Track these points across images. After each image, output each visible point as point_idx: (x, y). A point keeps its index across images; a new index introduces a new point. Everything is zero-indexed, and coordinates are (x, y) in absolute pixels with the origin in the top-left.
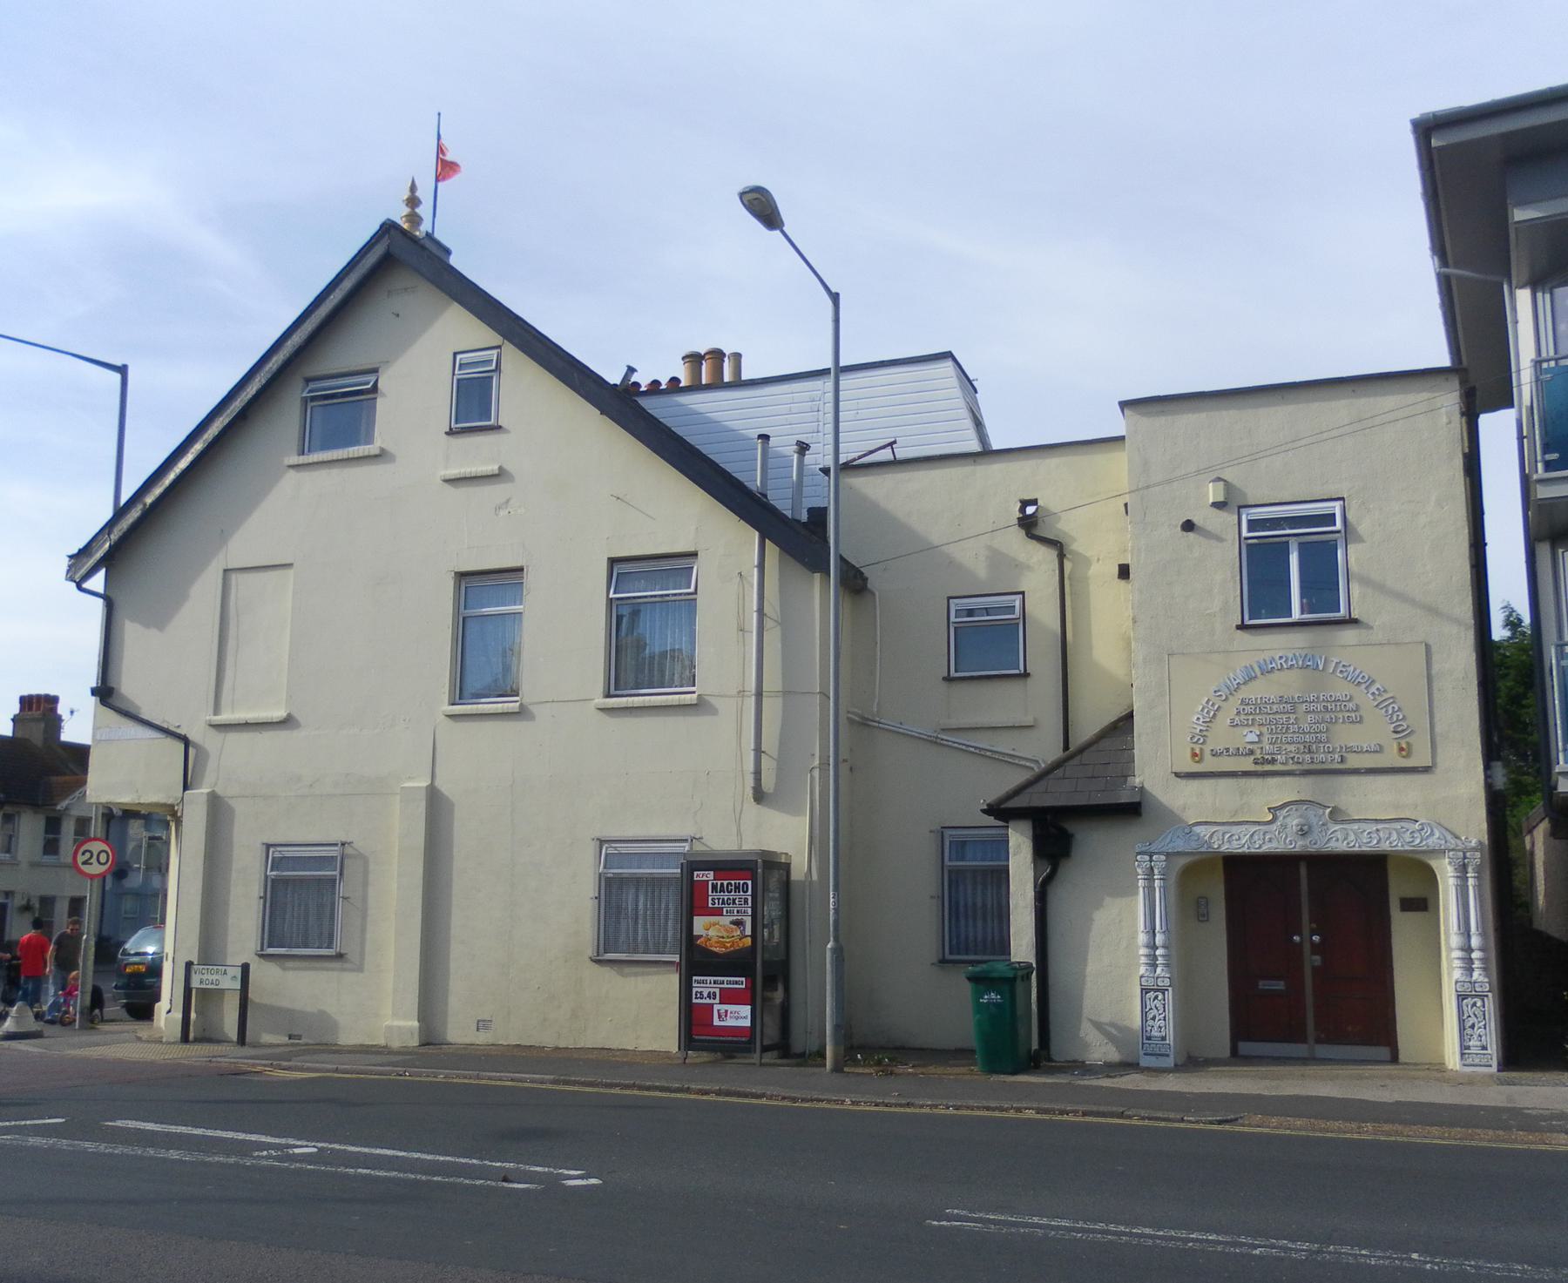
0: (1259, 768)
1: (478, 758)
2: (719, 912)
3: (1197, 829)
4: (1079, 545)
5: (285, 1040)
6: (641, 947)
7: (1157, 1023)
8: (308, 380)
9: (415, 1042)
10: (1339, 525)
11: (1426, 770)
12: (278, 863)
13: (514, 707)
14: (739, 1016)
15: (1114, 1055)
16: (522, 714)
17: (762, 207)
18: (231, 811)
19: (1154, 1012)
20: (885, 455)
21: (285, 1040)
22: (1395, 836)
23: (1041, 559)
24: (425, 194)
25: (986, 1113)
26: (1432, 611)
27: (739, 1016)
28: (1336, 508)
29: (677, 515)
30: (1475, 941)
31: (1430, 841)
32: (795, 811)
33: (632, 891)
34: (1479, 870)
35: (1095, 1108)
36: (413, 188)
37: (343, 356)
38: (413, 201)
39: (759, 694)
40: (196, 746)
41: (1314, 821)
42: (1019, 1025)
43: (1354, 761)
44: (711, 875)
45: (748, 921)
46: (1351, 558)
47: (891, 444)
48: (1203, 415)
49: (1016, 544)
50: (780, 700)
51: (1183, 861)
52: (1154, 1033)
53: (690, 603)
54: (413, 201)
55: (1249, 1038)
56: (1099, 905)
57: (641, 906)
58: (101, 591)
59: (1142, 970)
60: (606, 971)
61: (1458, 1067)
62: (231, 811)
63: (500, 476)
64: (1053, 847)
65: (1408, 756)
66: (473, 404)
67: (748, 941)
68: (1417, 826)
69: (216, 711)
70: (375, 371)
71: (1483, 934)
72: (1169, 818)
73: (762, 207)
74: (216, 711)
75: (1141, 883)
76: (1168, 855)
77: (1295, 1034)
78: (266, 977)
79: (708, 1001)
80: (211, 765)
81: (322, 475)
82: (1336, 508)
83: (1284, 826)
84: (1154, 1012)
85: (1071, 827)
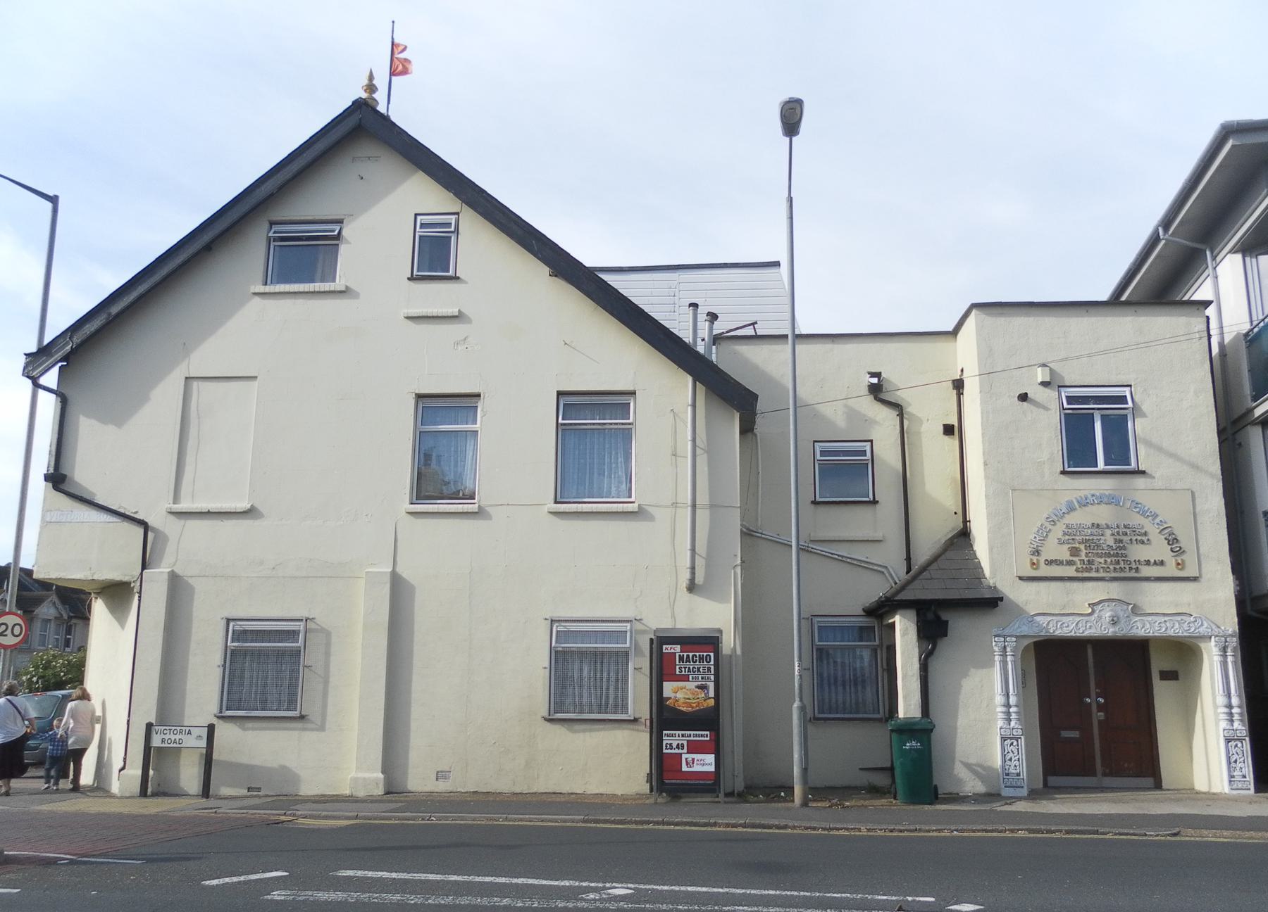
0: (1080, 575)
1: (437, 550)
2: (685, 678)
3: (1038, 619)
4: (912, 409)
5: (244, 792)
6: (586, 708)
7: (1013, 763)
8: (272, 224)
9: (380, 791)
10: (1130, 404)
11: (1195, 579)
12: (241, 635)
13: (474, 508)
14: (705, 763)
15: (980, 788)
16: (479, 514)
17: (791, 117)
18: (191, 590)
19: (1011, 755)
20: (749, 331)
21: (244, 792)
22: (1177, 626)
23: (886, 417)
24: (381, 82)
25: (985, 834)
26: (1195, 467)
27: (705, 763)
28: (1127, 391)
29: (616, 360)
30: (1235, 701)
31: (1201, 630)
32: (722, 599)
33: (577, 663)
34: (1234, 650)
35: (1074, 828)
36: (371, 77)
37: (311, 205)
38: (371, 88)
39: (694, 506)
40: (154, 530)
41: (1121, 614)
42: (914, 766)
43: (1146, 571)
44: (678, 648)
45: (711, 685)
46: (1138, 428)
47: (754, 324)
48: (1031, 319)
49: (869, 407)
50: (707, 512)
51: (1026, 642)
52: (1012, 770)
53: (626, 435)
54: (371, 88)
55: (1055, 774)
56: (966, 675)
57: (585, 673)
58: (54, 387)
59: (1000, 723)
60: (558, 730)
61: (1227, 790)
62: (192, 589)
63: (458, 318)
64: (932, 631)
65: (1182, 569)
66: (433, 257)
67: (711, 703)
68: (1192, 619)
69: (176, 499)
70: (340, 222)
71: (1240, 696)
72: (1017, 611)
73: (791, 117)
74: (176, 499)
75: (997, 658)
76: (1016, 637)
77: (1089, 771)
78: (225, 732)
79: (677, 751)
80: (170, 549)
81: (287, 303)
82: (1127, 391)
83: (1100, 617)
84: (1011, 755)
85: (945, 616)
